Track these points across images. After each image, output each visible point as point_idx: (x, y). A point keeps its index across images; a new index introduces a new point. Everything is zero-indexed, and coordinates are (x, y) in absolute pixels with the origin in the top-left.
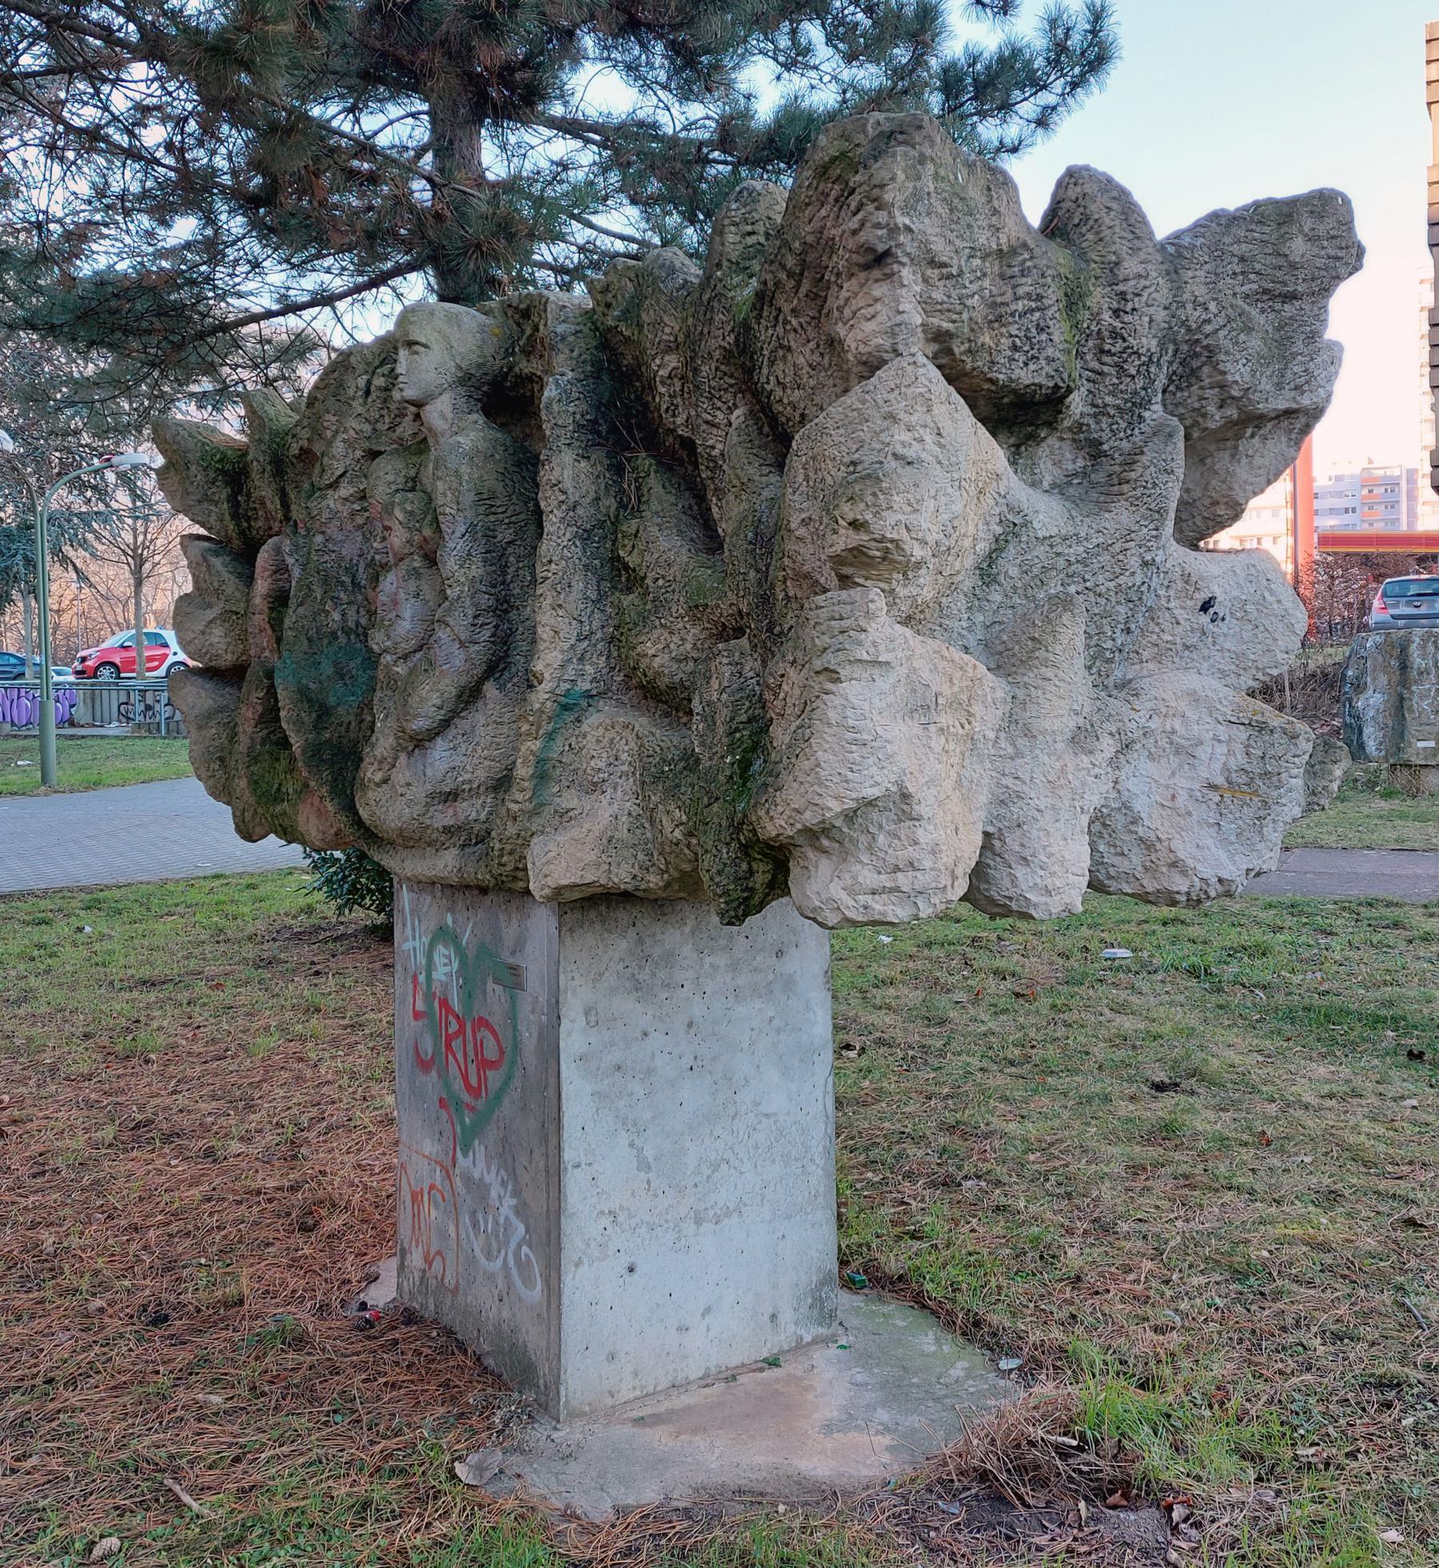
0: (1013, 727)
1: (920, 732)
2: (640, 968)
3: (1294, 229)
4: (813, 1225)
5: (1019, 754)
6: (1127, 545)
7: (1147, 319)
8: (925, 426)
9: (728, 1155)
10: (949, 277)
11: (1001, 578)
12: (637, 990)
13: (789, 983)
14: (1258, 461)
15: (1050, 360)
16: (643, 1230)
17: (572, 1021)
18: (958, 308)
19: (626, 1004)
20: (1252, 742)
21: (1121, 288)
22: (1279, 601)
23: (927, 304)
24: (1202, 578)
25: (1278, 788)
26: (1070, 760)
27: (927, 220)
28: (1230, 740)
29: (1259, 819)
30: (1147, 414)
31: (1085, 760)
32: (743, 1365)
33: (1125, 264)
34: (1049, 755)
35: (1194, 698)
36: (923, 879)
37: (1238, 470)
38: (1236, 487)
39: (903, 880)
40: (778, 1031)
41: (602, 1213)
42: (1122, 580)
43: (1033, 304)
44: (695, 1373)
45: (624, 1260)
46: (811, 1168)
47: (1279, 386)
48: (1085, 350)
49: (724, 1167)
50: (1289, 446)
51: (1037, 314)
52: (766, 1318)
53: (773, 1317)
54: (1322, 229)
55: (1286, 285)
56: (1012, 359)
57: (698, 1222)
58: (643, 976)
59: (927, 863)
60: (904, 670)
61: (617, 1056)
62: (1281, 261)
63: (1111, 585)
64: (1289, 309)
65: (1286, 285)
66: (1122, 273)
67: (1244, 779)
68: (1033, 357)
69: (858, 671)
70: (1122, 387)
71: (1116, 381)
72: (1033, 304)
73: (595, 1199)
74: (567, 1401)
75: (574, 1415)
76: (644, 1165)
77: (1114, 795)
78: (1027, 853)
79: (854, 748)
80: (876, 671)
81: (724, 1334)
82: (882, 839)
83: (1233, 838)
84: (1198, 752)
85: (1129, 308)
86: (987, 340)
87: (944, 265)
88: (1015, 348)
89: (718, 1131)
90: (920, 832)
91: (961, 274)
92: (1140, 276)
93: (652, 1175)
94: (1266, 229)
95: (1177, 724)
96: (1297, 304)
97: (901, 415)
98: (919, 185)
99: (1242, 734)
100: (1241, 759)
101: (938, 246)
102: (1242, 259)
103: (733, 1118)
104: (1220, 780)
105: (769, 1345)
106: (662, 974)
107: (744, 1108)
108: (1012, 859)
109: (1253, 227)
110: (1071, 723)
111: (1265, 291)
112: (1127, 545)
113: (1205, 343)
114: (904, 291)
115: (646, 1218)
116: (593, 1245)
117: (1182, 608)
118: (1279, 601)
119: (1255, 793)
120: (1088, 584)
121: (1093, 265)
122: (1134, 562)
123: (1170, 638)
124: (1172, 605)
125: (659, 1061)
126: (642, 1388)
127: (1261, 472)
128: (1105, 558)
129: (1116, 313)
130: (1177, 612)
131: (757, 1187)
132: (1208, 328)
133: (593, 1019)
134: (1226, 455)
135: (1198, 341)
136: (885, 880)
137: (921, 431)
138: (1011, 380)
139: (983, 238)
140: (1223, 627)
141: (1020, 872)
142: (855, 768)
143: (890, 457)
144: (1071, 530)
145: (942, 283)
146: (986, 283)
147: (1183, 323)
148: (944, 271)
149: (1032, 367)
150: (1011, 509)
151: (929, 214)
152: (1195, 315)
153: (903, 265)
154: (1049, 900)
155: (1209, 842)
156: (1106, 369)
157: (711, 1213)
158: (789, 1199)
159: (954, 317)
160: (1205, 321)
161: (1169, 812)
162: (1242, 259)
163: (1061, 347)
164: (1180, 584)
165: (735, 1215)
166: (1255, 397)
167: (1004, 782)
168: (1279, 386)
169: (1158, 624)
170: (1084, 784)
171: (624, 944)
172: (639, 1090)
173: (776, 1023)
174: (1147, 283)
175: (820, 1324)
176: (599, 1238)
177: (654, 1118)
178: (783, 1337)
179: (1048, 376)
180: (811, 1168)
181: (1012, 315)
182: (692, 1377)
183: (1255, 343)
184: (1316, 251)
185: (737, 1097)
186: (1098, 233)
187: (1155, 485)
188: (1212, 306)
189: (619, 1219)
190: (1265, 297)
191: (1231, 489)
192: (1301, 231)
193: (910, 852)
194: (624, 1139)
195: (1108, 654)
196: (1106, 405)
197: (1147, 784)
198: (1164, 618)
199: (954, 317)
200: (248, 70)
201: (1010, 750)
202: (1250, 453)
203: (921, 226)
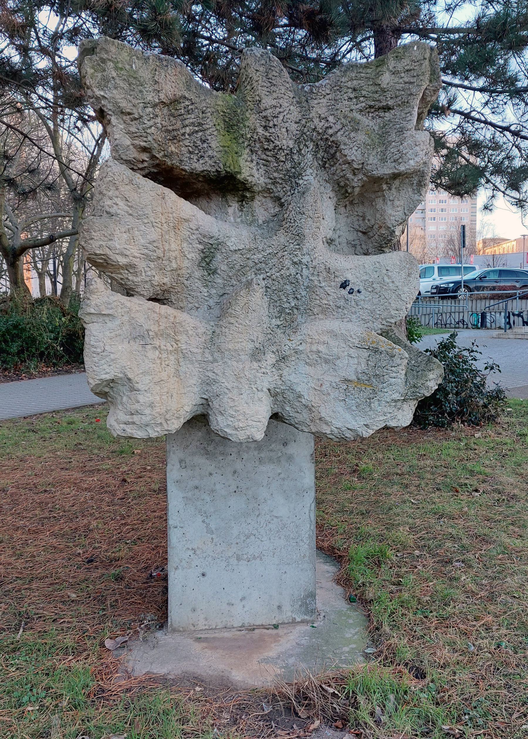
0: (213, 347)
1: (140, 349)
2: (208, 444)
3: (385, 68)
4: (302, 570)
5: (215, 361)
6: (284, 254)
7: (285, 130)
8: (117, 197)
9: (255, 532)
10: (136, 119)
11: (219, 271)
12: (206, 454)
13: (290, 458)
14: (397, 203)
15: (211, 157)
16: (210, 559)
17: (173, 465)
18: (145, 134)
19: (200, 460)
20: (370, 358)
21: (264, 114)
22: (393, 282)
23: (133, 135)
24: (337, 271)
25: (383, 383)
26: (248, 365)
27: (115, 92)
28: (358, 357)
29: (370, 399)
30: (301, 182)
31: (255, 365)
32: (262, 625)
33: (263, 101)
34: (237, 362)
35: (334, 334)
36: (145, 419)
37: (386, 208)
38: (387, 218)
39: (136, 418)
40: (283, 479)
41: (188, 549)
42: (283, 272)
43: (197, 129)
44: (237, 624)
45: (201, 571)
46: (301, 544)
47: (383, 160)
48: (256, 149)
49: (252, 537)
50: (415, 194)
51: (200, 134)
52: (275, 607)
53: (279, 607)
54: (400, 67)
55: (381, 102)
56: (190, 158)
57: (239, 559)
58: (210, 448)
59: (147, 411)
60: (126, 318)
61: (196, 482)
62: (377, 88)
63: (278, 274)
64: (388, 115)
65: (381, 102)
66: (262, 106)
67: (365, 378)
68: (201, 156)
69: (95, 318)
70: (280, 168)
71: (276, 165)
72: (197, 129)
73: (185, 542)
74: (171, 624)
75: (174, 630)
76: (210, 531)
77: (280, 382)
78: (221, 409)
79: (95, 355)
80: (106, 318)
81: (254, 610)
82: (125, 399)
83: (354, 408)
84: (338, 362)
85: (271, 124)
86: (174, 149)
87: (129, 114)
88: (190, 153)
89: (249, 521)
90: (139, 396)
91: (141, 117)
92: (275, 107)
93: (214, 536)
94: (369, 71)
95: (322, 348)
96: (392, 112)
97: (105, 192)
98: (105, 74)
99: (366, 354)
100: (363, 366)
101: (123, 104)
102: (355, 90)
103: (258, 516)
104: (353, 377)
105: (277, 619)
106: (221, 448)
107: (264, 512)
108: (216, 412)
109: (361, 70)
110: (251, 346)
111: (371, 107)
112: (284, 254)
113: (331, 139)
114: (114, 129)
115: (211, 554)
116: (184, 561)
117: (329, 286)
118: (393, 282)
119: (371, 385)
120: (268, 274)
121: (249, 103)
122: (287, 263)
123: (326, 302)
124: (323, 284)
125: (218, 487)
126: (210, 626)
127: (399, 209)
128: (275, 260)
129: (265, 128)
130: (326, 289)
131: (271, 548)
132: (330, 131)
133: (183, 465)
134: (380, 200)
135: (327, 139)
136: (128, 418)
137: (116, 199)
138: (192, 169)
139: (150, 97)
140: (361, 296)
141: (220, 418)
142: (97, 365)
143: (105, 213)
144: (253, 246)
145: (133, 123)
146: (158, 120)
147: (314, 130)
148: (131, 116)
149: (201, 162)
150: (204, 236)
151: (116, 88)
152: (320, 125)
153: (111, 115)
154: (237, 433)
155: (340, 409)
156: (269, 159)
157: (245, 557)
158: (289, 556)
159: (145, 139)
160: (327, 128)
161: (319, 392)
162: (355, 90)
163: (217, 150)
164: (325, 273)
165: (259, 559)
166: (369, 168)
167: (207, 374)
168: (383, 160)
169: (317, 295)
170: (255, 377)
171: (200, 434)
172: (208, 498)
173: (282, 476)
174: (281, 110)
175: (305, 614)
176: (187, 559)
177: (215, 512)
178: (285, 617)
179: (211, 166)
180: (301, 544)
181: (184, 134)
182: (235, 626)
183: (361, 137)
184: (397, 80)
185: (259, 507)
186: (252, 85)
187: (295, 221)
188: (331, 119)
189: (197, 553)
190: (372, 110)
191: (385, 219)
192: (388, 69)
193: (137, 406)
194: (200, 519)
195: (287, 311)
196: (275, 178)
197: (302, 379)
198: (319, 291)
199: (145, 139)
200: (379, 52)
201: (210, 358)
202: (391, 198)
203: (111, 95)
